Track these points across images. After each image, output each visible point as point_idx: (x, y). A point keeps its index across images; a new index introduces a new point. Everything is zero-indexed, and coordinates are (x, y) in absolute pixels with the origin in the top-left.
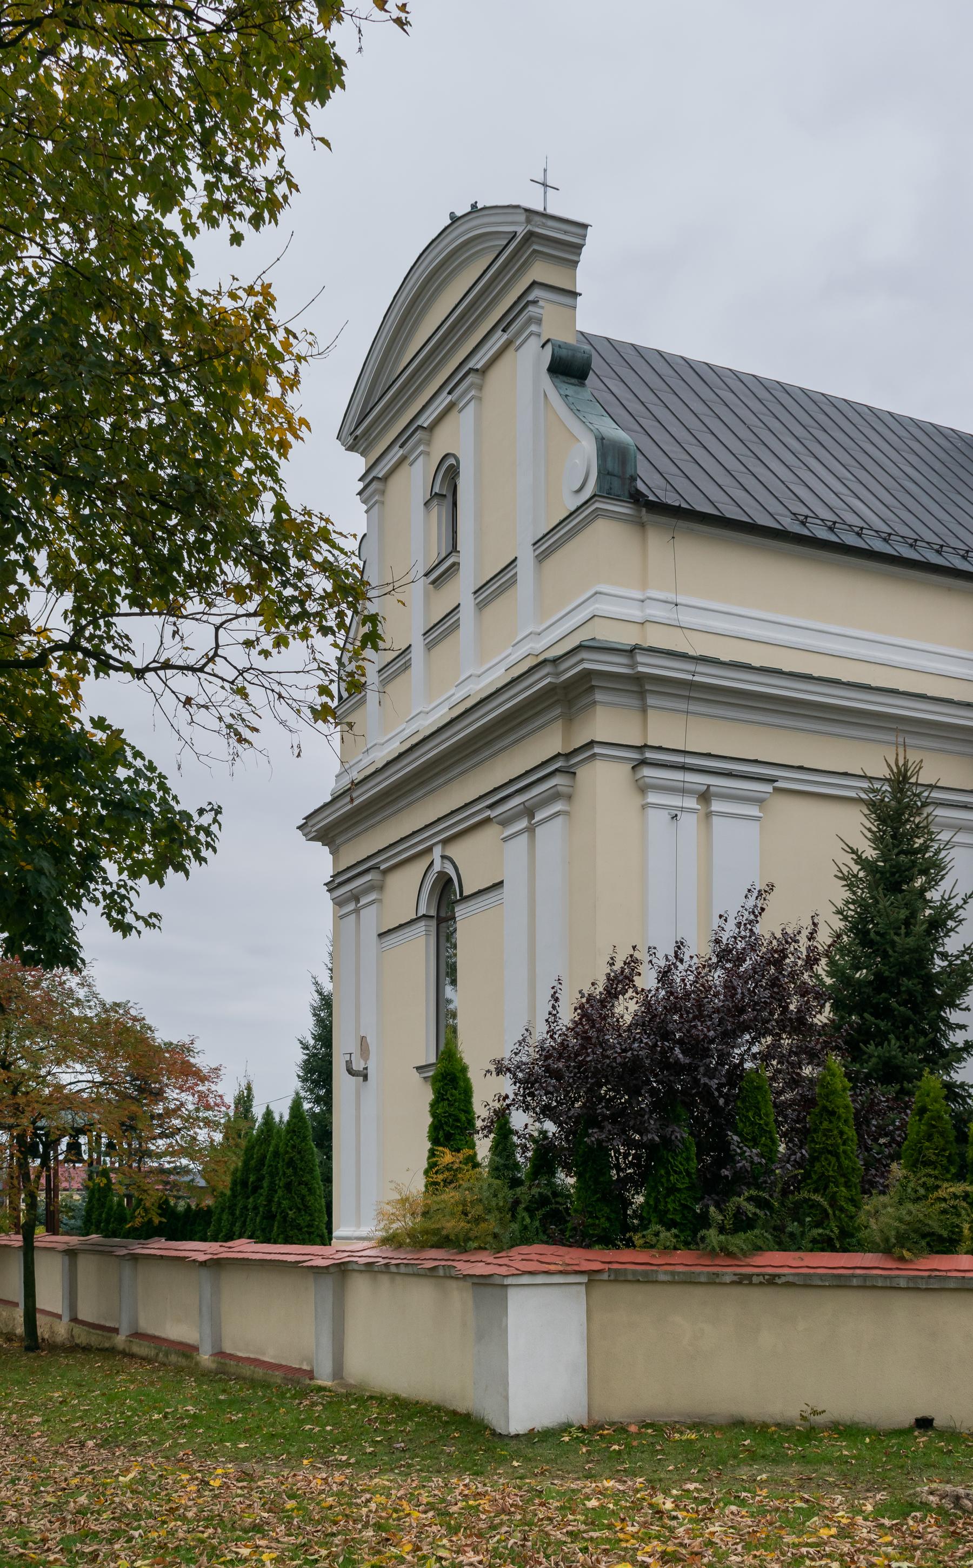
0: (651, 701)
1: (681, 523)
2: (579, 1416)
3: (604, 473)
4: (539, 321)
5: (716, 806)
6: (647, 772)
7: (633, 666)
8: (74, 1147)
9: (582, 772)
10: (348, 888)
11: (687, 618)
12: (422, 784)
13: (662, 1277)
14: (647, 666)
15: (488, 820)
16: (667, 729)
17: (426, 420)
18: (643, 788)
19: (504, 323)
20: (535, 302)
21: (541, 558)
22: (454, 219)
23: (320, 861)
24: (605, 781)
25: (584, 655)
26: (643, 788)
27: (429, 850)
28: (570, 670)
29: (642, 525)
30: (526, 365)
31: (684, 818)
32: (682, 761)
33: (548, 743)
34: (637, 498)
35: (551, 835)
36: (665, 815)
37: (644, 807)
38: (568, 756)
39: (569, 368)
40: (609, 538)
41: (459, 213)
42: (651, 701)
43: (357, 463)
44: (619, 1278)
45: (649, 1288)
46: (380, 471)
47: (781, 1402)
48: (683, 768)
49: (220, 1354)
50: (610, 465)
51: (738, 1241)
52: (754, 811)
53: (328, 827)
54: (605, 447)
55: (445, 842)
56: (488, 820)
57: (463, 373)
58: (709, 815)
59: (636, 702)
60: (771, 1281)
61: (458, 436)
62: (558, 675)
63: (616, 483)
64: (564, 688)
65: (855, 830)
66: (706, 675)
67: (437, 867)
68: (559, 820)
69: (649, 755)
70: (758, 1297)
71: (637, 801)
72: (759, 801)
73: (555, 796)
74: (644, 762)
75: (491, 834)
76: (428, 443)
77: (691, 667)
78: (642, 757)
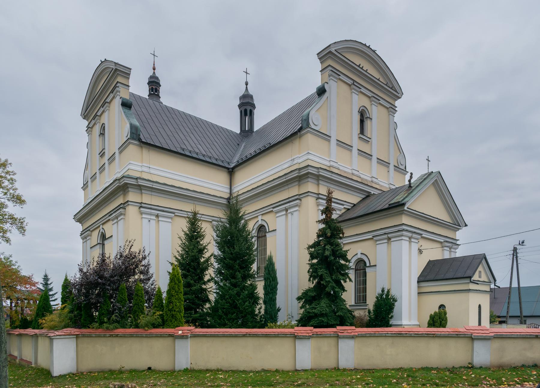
0: (320, 182)
1: (151, 147)
2: (74, 371)
3: (132, 133)
4: (119, 92)
5: (160, 219)
6: (142, 209)
7: (138, 182)
8: (29, 303)
9: (127, 208)
10: (85, 235)
11: (152, 171)
12: (98, 209)
13: (94, 336)
14: (141, 182)
15: (109, 220)
16: (147, 199)
17: (99, 114)
18: (142, 213)
19: (112, 92)
20: (118, 87)
21: (120, 153)
22: (102, 62)
23: (79, 227)
24: (132, 211)
25: (125, 179)
26: (142, 213)
27: (99, 226)
28: (304, 172)
29: (142, 147)
30: (117, 103)
31: (151, 221)
32: (151, 207)
33: (294, 191)
34: (140, 140)
35: (121, 223)
36: (147, 220)
37: (142, 218)
38: (124, 204)
39: (126, 105)
40: (133, 149)
41: (103, 61)
42: (320, 182)
43: (86, 123)
44: (84, 336)
45: (90, 338)
46: (91, 126)
47: (115, 365)
48: (151, 209)
49: (22, 359)
50: (133, 131)
51: (111, 327)
52: (170, 220)
53: (81, 218)
54: (132, 126)
55: (103, 224)
56: (109, 220)
57: (105, 103)
58: (159, 221)
59: (316, 182)
60: (117, 336)
61: (105, 119)
62: (120, 183)
63: (135, 136)
64: (122, 187)
65: (183, 225)
66: (156, 186)
67: (260, 222)
68: (122, 220)
69: (143, 205)
70: (115, 340)
71: (140, 216)
72: (171, 218)
73: (121, 214)
74: (141, 207)
75: (111, 223)
76: (100, 120)
77: (152, 184)
78: (141, 205)
